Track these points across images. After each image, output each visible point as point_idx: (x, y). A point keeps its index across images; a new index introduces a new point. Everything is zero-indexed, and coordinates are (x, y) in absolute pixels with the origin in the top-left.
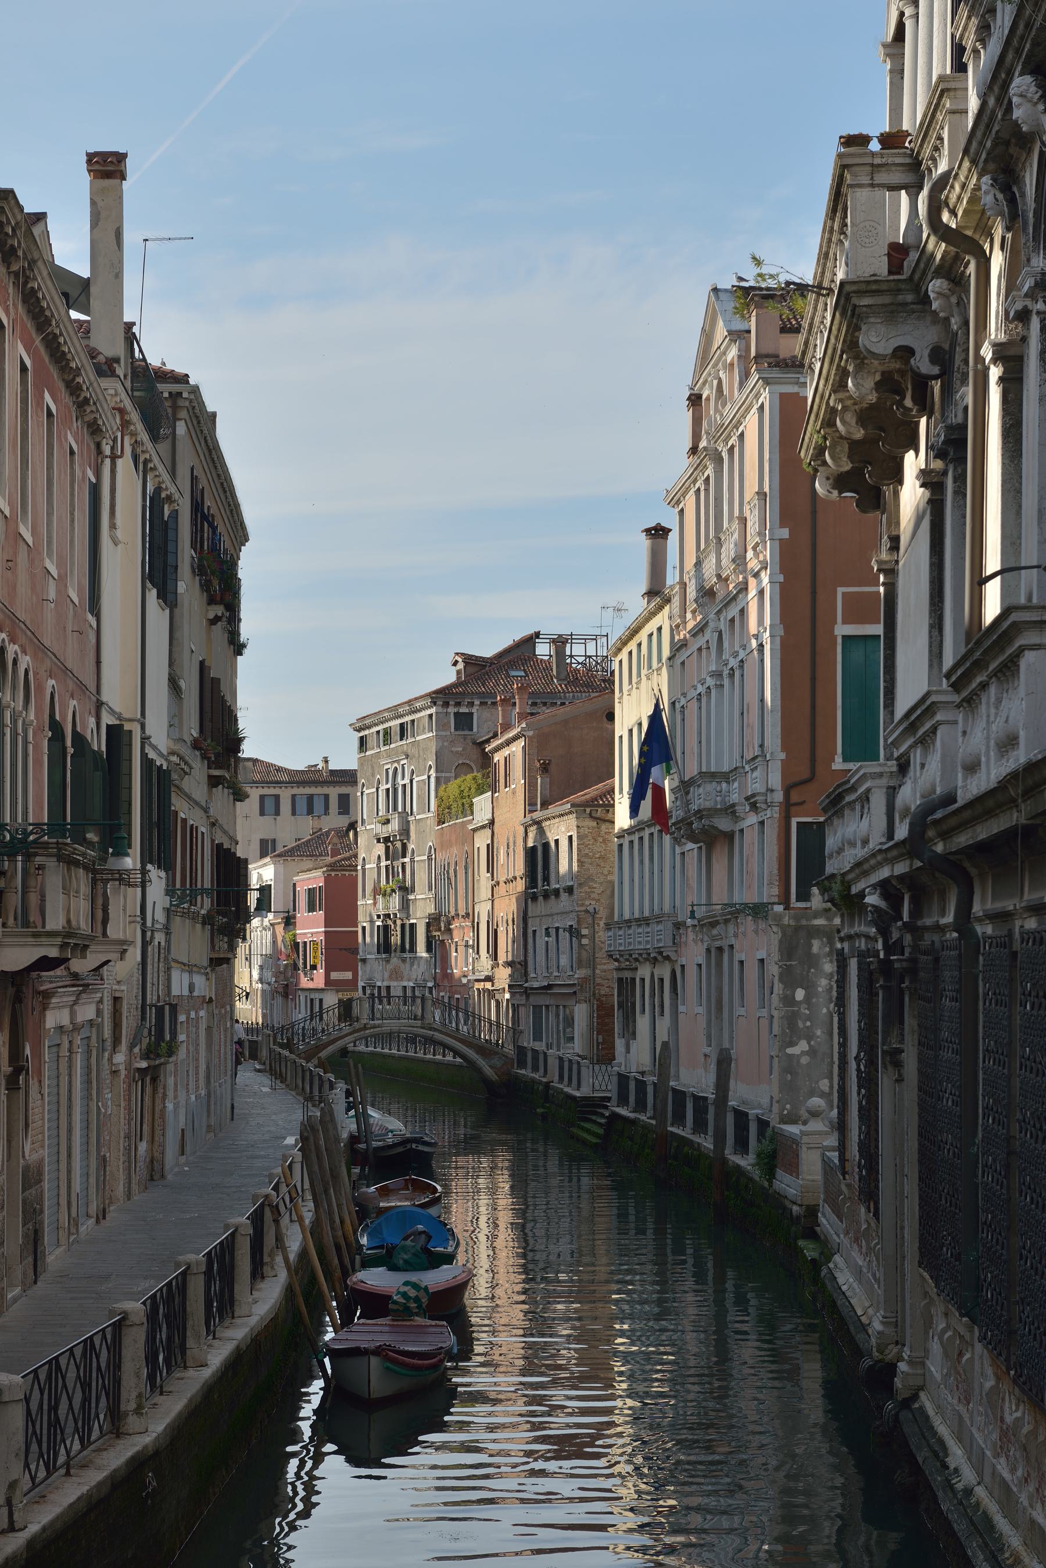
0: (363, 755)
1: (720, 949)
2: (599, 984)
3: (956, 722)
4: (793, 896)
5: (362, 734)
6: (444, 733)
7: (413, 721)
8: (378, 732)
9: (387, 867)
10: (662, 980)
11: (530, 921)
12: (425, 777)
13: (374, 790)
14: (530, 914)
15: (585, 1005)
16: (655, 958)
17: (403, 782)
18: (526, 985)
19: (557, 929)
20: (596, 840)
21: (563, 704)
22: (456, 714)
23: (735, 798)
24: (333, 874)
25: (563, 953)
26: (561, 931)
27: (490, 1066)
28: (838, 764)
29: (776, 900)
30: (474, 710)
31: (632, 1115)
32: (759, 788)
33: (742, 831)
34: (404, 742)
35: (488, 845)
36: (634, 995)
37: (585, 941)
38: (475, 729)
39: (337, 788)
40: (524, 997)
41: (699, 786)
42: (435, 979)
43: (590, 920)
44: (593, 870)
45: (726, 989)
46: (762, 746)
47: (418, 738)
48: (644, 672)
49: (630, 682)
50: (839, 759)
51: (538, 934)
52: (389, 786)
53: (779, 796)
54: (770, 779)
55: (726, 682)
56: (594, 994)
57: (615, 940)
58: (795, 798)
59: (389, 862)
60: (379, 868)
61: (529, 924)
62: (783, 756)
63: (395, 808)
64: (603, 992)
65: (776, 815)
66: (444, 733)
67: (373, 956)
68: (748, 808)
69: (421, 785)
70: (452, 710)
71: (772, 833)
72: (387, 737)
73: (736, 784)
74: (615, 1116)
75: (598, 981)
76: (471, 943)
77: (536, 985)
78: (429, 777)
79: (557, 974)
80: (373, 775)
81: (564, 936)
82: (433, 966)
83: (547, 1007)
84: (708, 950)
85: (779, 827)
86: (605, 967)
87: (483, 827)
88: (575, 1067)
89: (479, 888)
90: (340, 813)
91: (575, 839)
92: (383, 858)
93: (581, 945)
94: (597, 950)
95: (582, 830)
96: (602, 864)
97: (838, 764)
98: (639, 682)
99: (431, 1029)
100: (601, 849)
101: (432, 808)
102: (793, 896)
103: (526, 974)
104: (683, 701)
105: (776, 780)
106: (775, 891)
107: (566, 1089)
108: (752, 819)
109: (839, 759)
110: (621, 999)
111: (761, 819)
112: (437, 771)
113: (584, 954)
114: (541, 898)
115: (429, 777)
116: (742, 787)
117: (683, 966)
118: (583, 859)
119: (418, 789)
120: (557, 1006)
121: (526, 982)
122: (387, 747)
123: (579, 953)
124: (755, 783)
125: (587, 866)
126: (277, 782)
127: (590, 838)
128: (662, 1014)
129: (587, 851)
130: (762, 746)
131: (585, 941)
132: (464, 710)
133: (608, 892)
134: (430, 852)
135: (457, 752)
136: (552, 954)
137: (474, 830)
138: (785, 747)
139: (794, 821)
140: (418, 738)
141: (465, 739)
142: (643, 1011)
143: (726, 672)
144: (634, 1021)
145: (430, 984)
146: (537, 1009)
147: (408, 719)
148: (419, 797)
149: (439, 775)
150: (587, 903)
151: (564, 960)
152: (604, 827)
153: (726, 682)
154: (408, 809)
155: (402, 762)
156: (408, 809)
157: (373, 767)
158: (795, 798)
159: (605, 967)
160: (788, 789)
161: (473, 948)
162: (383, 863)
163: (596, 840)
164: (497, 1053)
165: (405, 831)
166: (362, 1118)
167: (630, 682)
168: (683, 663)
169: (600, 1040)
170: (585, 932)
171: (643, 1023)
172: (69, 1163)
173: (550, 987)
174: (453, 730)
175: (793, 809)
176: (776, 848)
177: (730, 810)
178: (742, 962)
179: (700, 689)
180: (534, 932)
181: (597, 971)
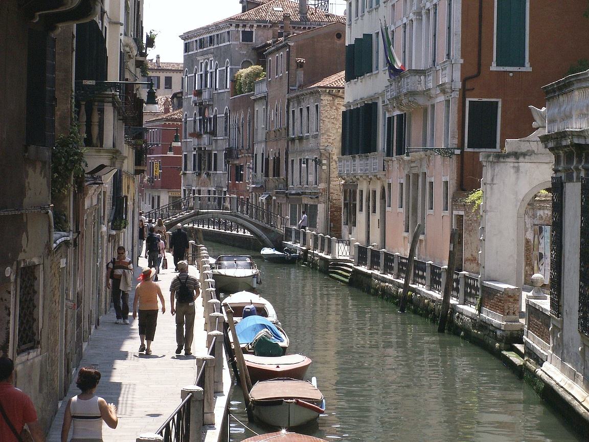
0: (187, 54)
1: (416, 176)
4: (466, 145)
5: (187, 41)
7: (218, 35)
8: (196, 41)
9: (200, 120)
10: (374, 192)
12: (225, 68)
13: (193, 75)
16: (371, 179)
17: (211, 71)
19: (307, 160)
20: (331, 108)
21: (304, 28)
22: (243, 32)
23: (430, 85)
25: (311, 174)
26: (310, 161)
28: (494, 67)
29: (456, 146)
30: (254, 30)
31: (370, 272)
32: (447, 80)
33: (433, 106)
34: (212, 47)
36: (355, 200)
38: (254, 41)
39: (165, 73)
40: (285, 199)
41: (407, 78)
42: (228, 186)
45: (420, 199)
46: (448, 55)
47: (220, 45)
48: (366, 10)
49: (357, 16)
50: (494, 64)
51: (295, 162)
52: (202, 72)
53: (458, 85)
54: (451, 76)
55: (424, 17)
56: (329, 198)
57: (344, 167)
58: (468, 86)
60: (195, 122)
61: (289, 156)
62: (462, 61)
63: (206, 86)
65: (458, 96)
67: (191, 172)
68: (438, 92)
70: (241, 29)
71: (454, 108)
72: (202, 44)
73: (431, 78)
74: (356, 272)
75: (332, 191)
76: (251, 166)
77: (293, 192)
78: (227, 68)
79: (307, 186)
80: (193, 66)
81: (312, 164)
82: (227, 179)
84: (408, 176)
85: (459, 103)
87: (261, 98)
88: (326, 241)
89: (257, 134)
90: (166, 88)
92: (198, 114)
97: (494, 67)
98: (362, 16)
101: (228, 87)
102: (466, 145)
103: (287, 185)
104: (393, 28)
105: (457, 75)
106: (456, 141)
107: (320, 254)
108: (442, 98)
109: (494, 64)
110: (354, 202)
111: (447, 98)
112: (231, 65)
114: (297, 141)
115: (227, 68)
116: (437, 79)
122: (201, 50)
124: (444, 79)
127: (328, 107)
128: (374, 211)
130: (448, 55)
132: (247, 29)
136: (304, 174)
137: (255, 100)
138: (462, 57)
139: (468, 100)
140: (220, 45)
142: (361, 210)
143: (423, 12)
144: (355, 215)
145: (225, 189)
147: (215, 33)
152: (337, 101)
153: (424, 17)
155: (210, 59)
158: (468, 86)
160: (464, 80)
161: (252, 169)
162: (198, 118)
163: (331, 108)
166: (471, 291)
167: (357, 16)
168: (393, 6)
169: (332, 226)
171: (361, 217)
172: (106, 294)
174: (241, 41)
175: (467, 93)
176: (456, 115)
177: (426, 93)
178: (431, 183)
179: (405, 20)
180: (293, 161)
181: (331, 185)
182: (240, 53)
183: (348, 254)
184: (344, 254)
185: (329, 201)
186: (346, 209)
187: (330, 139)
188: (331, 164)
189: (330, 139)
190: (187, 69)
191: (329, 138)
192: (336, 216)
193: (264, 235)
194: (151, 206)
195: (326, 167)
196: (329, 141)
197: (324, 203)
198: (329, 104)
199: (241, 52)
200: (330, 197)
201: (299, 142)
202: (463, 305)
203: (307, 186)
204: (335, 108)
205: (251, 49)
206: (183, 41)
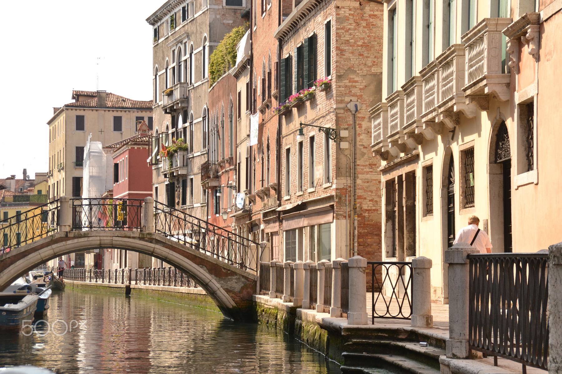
2: (360, 197)
3: (394, 255)
6: (216, 7)
11: (284, 141)
14: (284, 132)
15: (343, 222)
18: (279, 209)
20: (358, 24)
24: (136, 147)
27: (228, 291)
35: (247, 84)
37: (344, 145)
40: (277, 224)
43: (350, 120)
44: (354, 60)
56: (355, 209)
59: (174, 129)
61: (283, 144)
64: (365, 207)
66: (216, 7)
69: (198, 57)
75: (359, 192)
77: (289, 207)
78: (204, 47)
79: (312, 190)
80: (164, 59)
81: (320, 138)
82: (206, 214)
83: (301, 229)
86: (368, 176)
89: (240, 130)
91: (333, 23)
92: (170, 127)
93: (339, 149)
94: (358, 156)
95: (341, 12)
96: (366, 54)
99: (151, 240)
100: (363, 35)
101: (206, 76)
112: (210, 41)
113: (344, 160)
115: (204, 47)
117: (527, 109)
118: (343, 47)
119: (196, 61)
120: (312, 227)
121: (280, 205)
123: (338, 159)
125: (347, 55)
126: (123, 108)
127: (351, 21)
129: (347, 37)
131: (344, 145)
133: (372, 87)
134: (205, 113)
135: (228, 24)
141: (235, 13)
142: (428, 210)
146: (290, 233)
148: (196, 67)
149: (212, 44)
150: (347, 99)
151: (319, 172)
154: (189, 81)
156: (189, 81)
157: (163, 52)
159: (368, 176)
162: (170, 132)
163: (358, 24)
164: (233, 273)
165: (186, 99)
170: (344, 134)
173: (303, 206)
174: (224, 4)
181: (359, 182)
182: (224, 24)
183: (406, 312)
184: (394, 311)
185: (355, 212)
186: (390, 223)
187: (355, 87)
188: (358, 139)
189: (355, 87)
190: (157, 65)
191: (352, 86)
192: (370, 245)
193: (214, 281)
194: (118, 264)
195: (347, 143)
196: (354, 91)
197: (345, 217)
198: (353, 15)
199: (224, 21)
200: (358, 205)
201: (299, 110)
202: (467, 358)
203: (312, 190)
204: (364, 24)
205: (240, 18)
206: (151, 26)
